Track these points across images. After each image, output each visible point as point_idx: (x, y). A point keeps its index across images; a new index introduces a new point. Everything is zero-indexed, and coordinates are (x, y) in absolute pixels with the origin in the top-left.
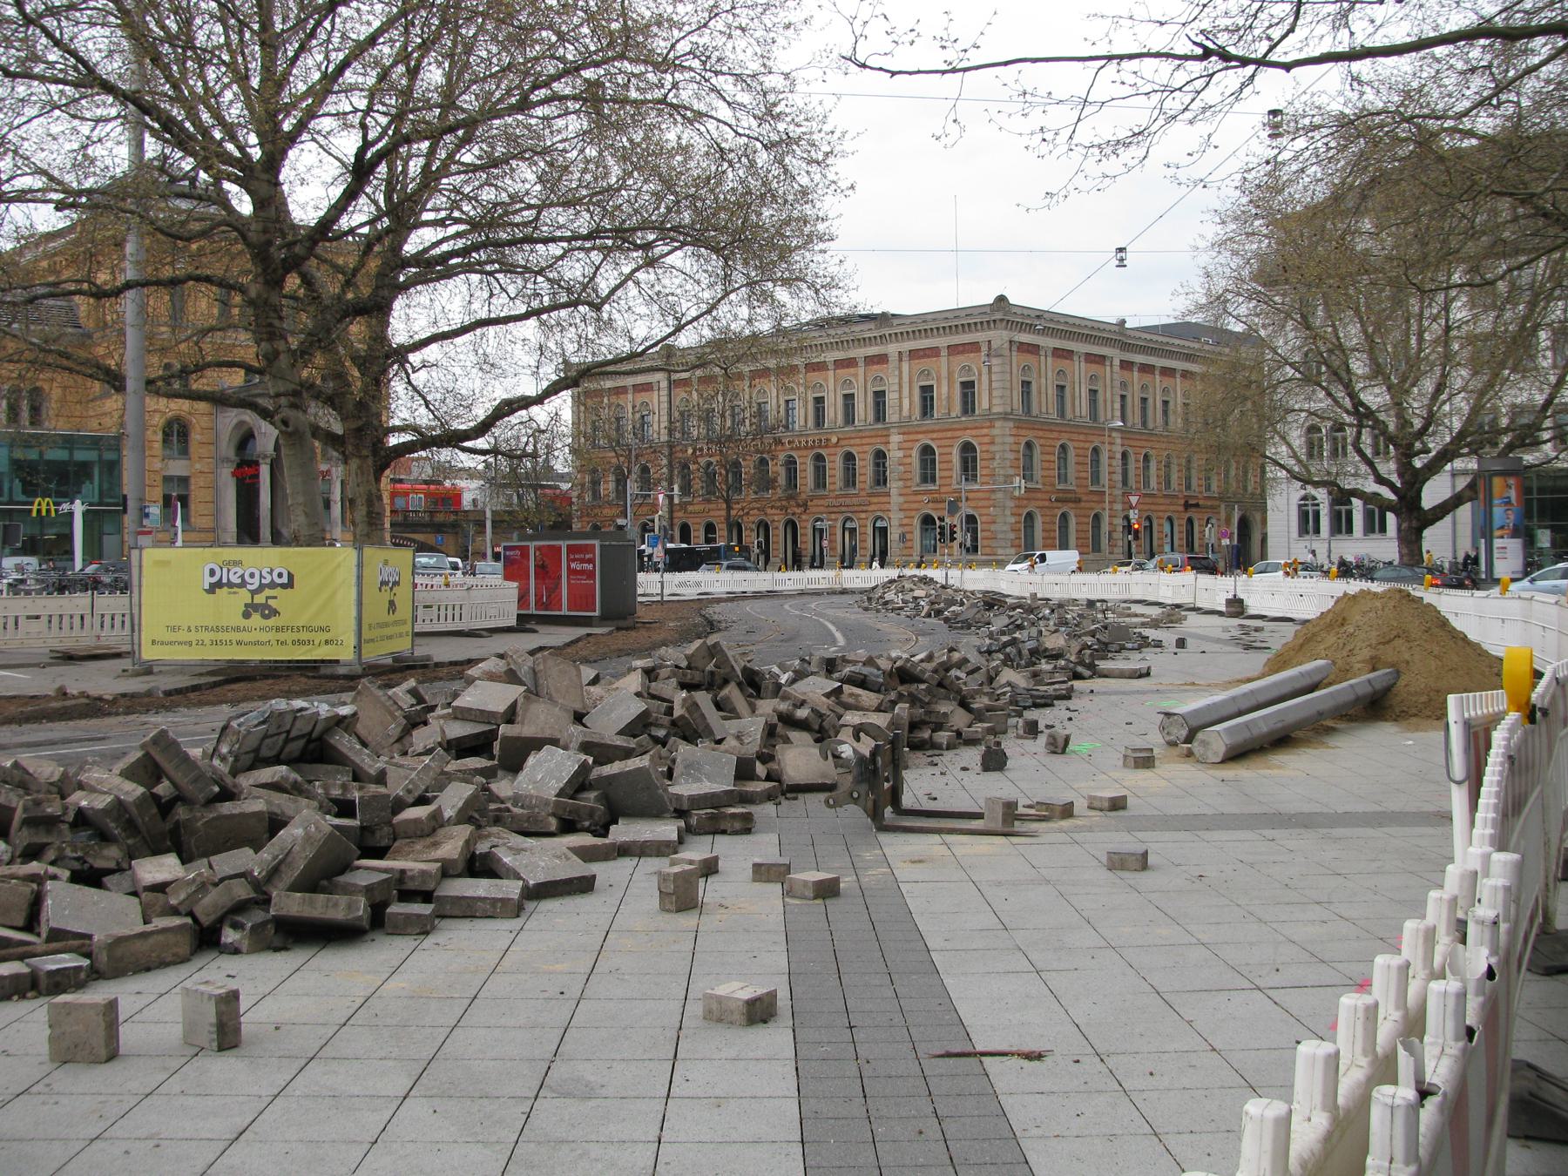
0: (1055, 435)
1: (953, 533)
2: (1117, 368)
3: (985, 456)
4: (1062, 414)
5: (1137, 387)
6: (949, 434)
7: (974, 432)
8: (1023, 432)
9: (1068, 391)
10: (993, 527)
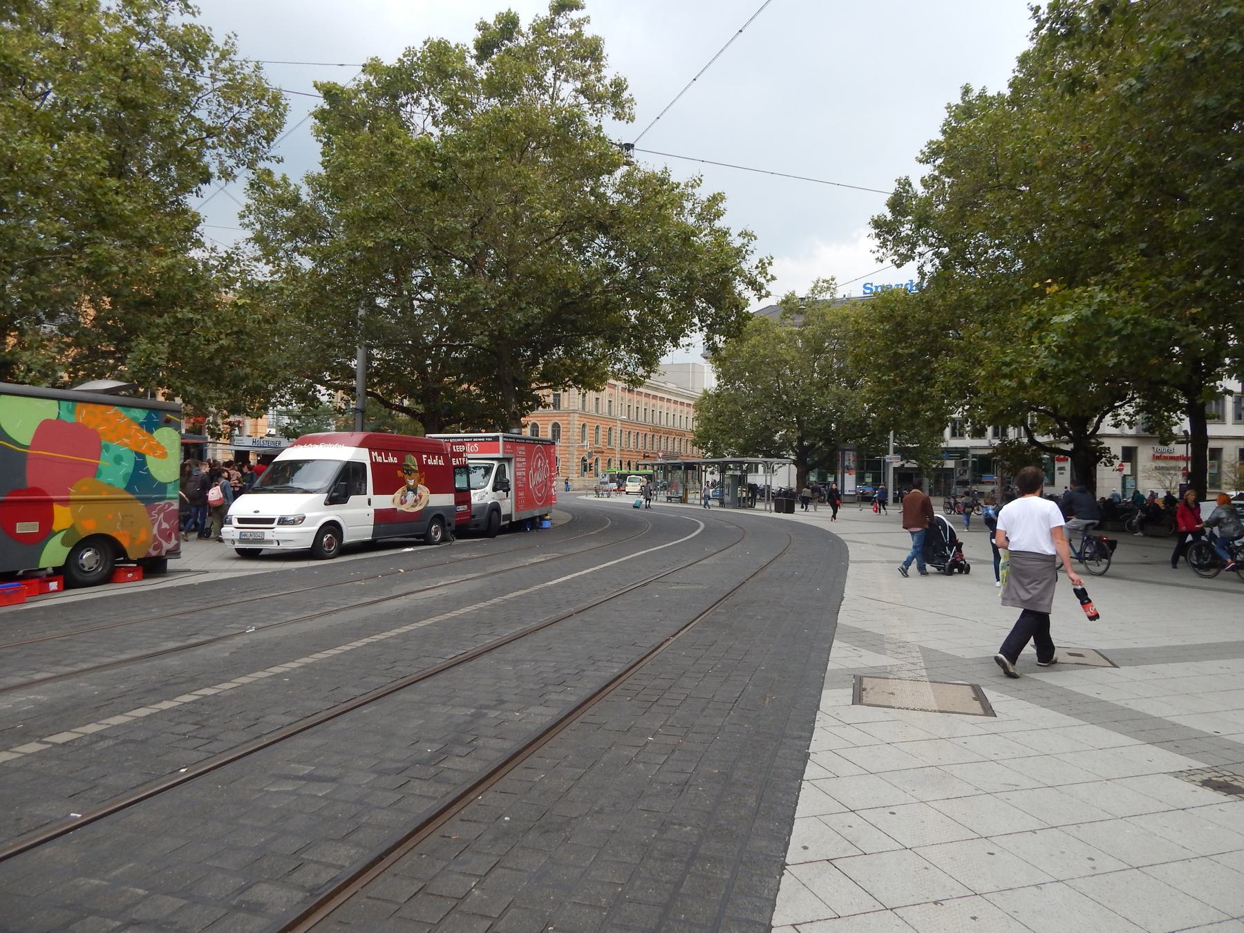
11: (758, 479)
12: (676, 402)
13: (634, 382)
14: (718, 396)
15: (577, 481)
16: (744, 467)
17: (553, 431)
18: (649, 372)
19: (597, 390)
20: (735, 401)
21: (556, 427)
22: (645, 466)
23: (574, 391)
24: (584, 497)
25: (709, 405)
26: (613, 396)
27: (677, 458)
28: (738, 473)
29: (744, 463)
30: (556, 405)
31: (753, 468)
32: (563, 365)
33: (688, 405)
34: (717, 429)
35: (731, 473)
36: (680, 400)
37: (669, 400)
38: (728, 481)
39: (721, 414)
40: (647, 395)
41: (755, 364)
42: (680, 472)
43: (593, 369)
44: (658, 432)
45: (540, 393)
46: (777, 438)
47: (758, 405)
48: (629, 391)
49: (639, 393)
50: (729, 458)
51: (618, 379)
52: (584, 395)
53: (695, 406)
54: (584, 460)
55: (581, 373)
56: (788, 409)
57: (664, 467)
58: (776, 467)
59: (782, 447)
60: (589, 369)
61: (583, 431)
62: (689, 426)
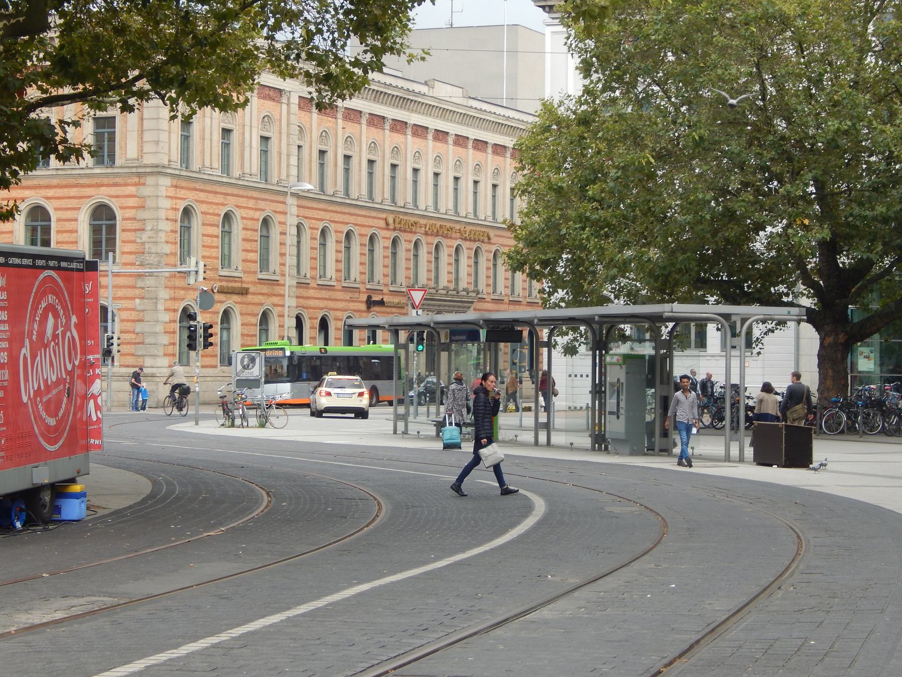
0: (219, 199)
1: (208, 336)
2: (295, 108)
3: (130, 225)
4: (226, 167)
5: (315, 135)
6: (73, 192)
7: (113, 191)
8: (182, 193)
9: (235, 137)
10: (139, 327)
11: (706, 362)
12: (460, 140)
13: (334, 83)
14: (584, 121)
16: (665, 330)
17: (96, 230)
18: (378, 52)
19: (226, 106)
20: (634, 138)
21: (103, 217)
22: (373, 330)
23: (155, 110)
25: (559, 149)
26: (273, 118)
27: (464, 306)
28: (647, 349)
30: (104, 149)
31: (691, 335)
32: (121, 30)
33: (499, 149)
34: (584, 221)
35: (624, 349)
36: (473, 133)
37: (440, 135)
39: (596, 175)
40: (376, 120)
41: (695, 27)
42: (473, 348)
43: (209, 43)
44: (409, 228)
45: (52, 114)
46: (759, 244)
47: (702, 147)
49: (353, 115)
50: (619, 306)
51: (287, 73)
52: (187, 122)
53: (518, 151)
54: (188, 315)
55: (177, 57)
56: (791, 157)
57: (425, 334)
59: (774, 272)
60: (199, 42)
61: (186, 229)
62: (504, 213)
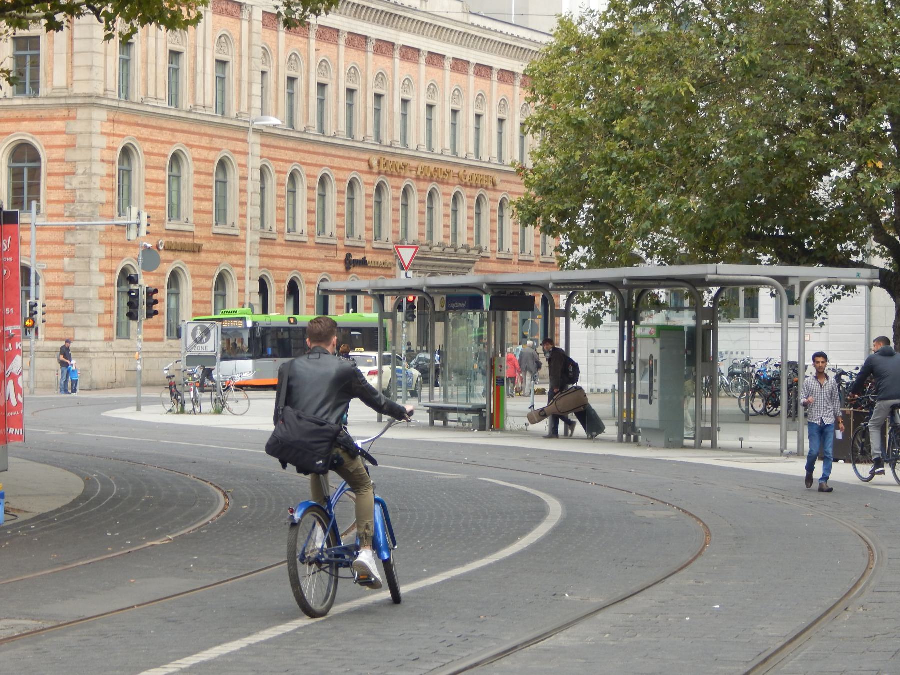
12: (460, 65)
14: (610, 42)
15: (103, 352)
19: (174, 23)
20: (671, 62)
22: (353, 298)
23: (88, 27)
24: (128, 414)
27: (464, 266)
28: (686, 320)
29: (700, 283)
31: (740, 302)
33: (507, 76)
34: (610, 163)
35: (658, 319)
36: (474, 56)
37: (435, 59)
38: (648, 350)
39: (624, 107)
40: (358, 41)
42: (474, 317)
44: (398, 172)
46: (822, 192)
47: (754, 74)
48: (289, 24)
49: (329, 34)
50: (652, 267)
52: (126, 42)
54: (127, 277)
58: (820, 298)
59: (840, 227)
61: (125, 174)
62: (512, 154)
